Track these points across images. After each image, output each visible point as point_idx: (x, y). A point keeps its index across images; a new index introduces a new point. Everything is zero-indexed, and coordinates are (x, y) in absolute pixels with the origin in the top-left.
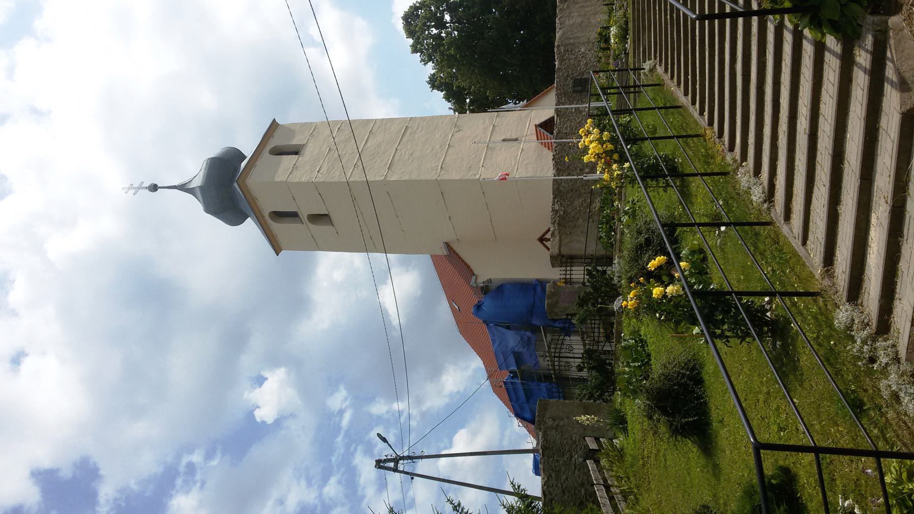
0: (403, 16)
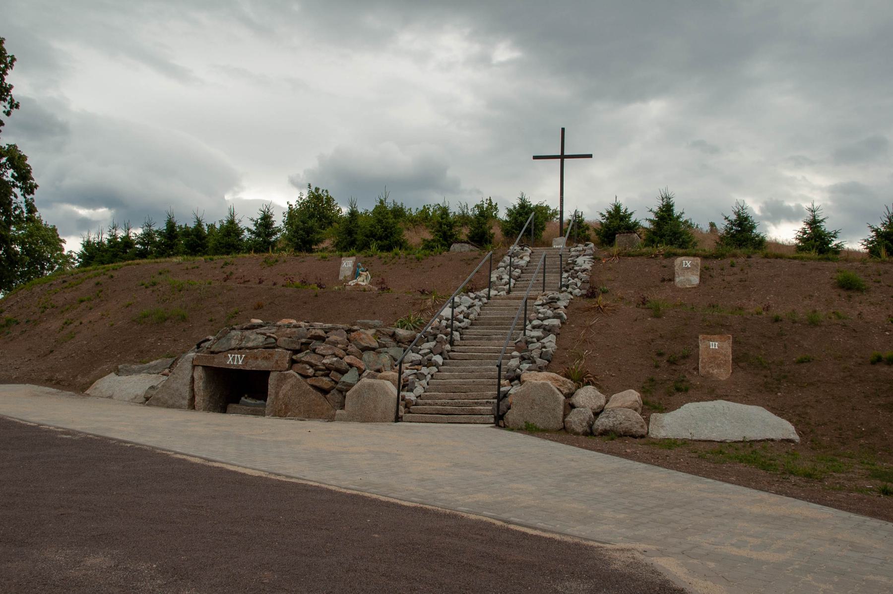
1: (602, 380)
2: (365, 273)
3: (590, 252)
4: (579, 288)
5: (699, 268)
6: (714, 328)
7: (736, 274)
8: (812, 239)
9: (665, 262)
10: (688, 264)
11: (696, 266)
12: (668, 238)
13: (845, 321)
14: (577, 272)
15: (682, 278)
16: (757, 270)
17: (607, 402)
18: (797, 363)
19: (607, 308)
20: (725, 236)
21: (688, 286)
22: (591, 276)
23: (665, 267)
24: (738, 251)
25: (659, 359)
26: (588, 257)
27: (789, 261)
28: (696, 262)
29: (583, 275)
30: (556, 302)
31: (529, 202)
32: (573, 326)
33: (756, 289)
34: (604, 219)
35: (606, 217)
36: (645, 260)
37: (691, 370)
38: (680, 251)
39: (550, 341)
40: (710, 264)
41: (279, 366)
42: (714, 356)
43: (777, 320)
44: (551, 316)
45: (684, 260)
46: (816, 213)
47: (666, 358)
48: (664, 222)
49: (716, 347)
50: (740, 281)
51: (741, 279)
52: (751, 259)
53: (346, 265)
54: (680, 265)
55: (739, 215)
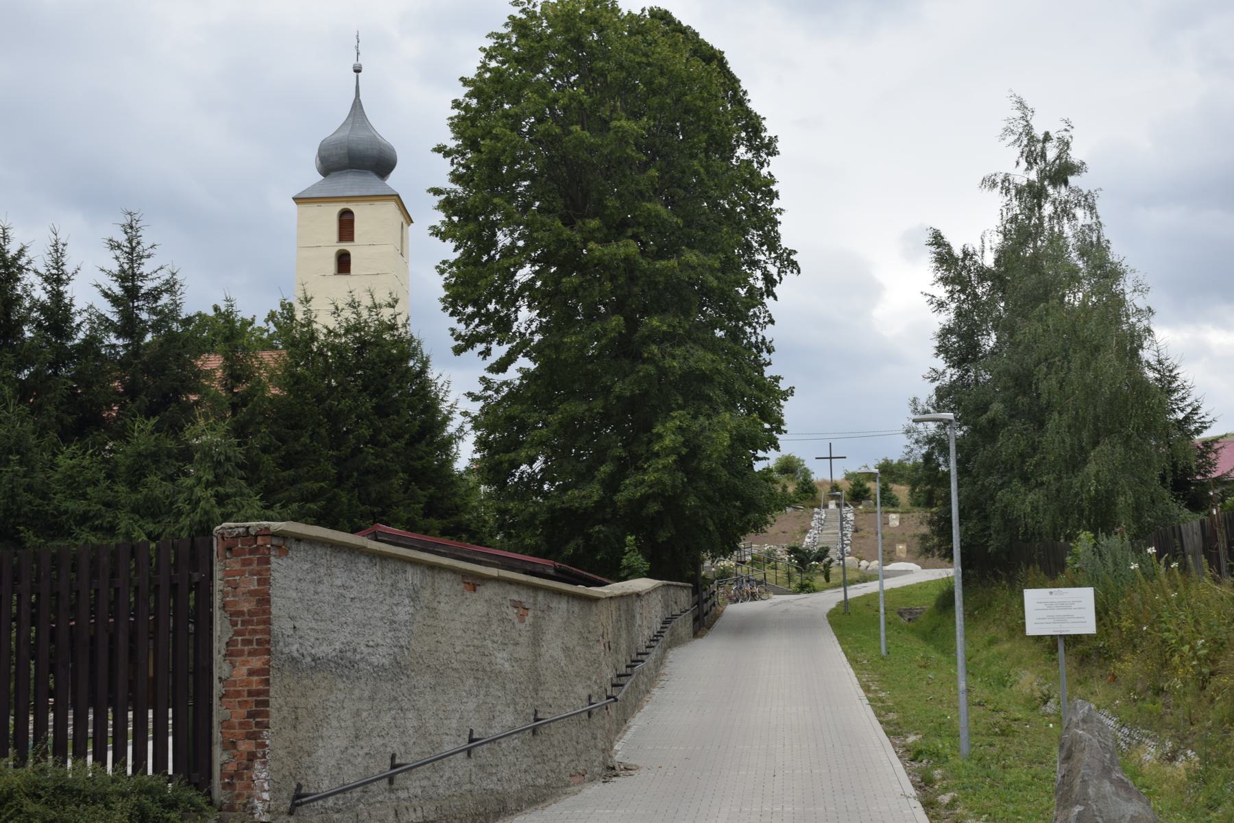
6: (901, 542)
9: (885, 515)
29: (852, 523)
42: (901, 550)
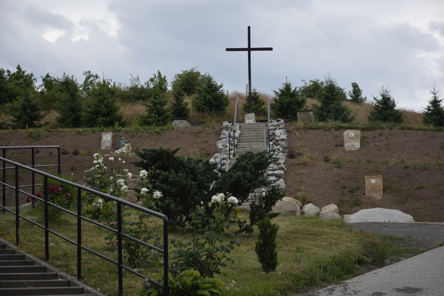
0: (181, 73)
1: (315, 202)
2: (127, 144)
3: (282, 126)
4: (282, 152)
5: (360, 137)
7: (383, 141)
8: (434, 115)
9: (336, 133)
10: (353, 135)
11: (357, 136)
12: (333, 114)
13: (441, 167)
14: (278, 141)
15: (349, 144)
16: (396, 138)
17: (321, 211)
18: (416, 189)
19: (309, 163)
20: (374, 112)
21: (353, 150)
22: (288, 143)
23: (337, 137)
24: (384, 125)
25: (344, 190)
26: (282, 130)
27: (416, 132)
28: (357, 133)
29: (283, 143)
30: (278, 160)
31: (215, 82)
32: (291, 174)
33: (395, 150)
34: (278, 96)
35: (279, 94)
36: (323, 131)
37: (361, 195)
38: (346, 125)
39: (282, 182)
40: (366, 134)
41: (132, 200)
42: (373, 187)
43: (406, 167)
44: (277, 168)
45: (350, 132)
46: (436, 95)
47: (347, 189)
48: (329, 100)
49: (375, 182)
50: (386, 146)
51: (386, 144)
52: (392, 131)
53: (106, 138)
54: (347, 135)
55: (383, 96)
